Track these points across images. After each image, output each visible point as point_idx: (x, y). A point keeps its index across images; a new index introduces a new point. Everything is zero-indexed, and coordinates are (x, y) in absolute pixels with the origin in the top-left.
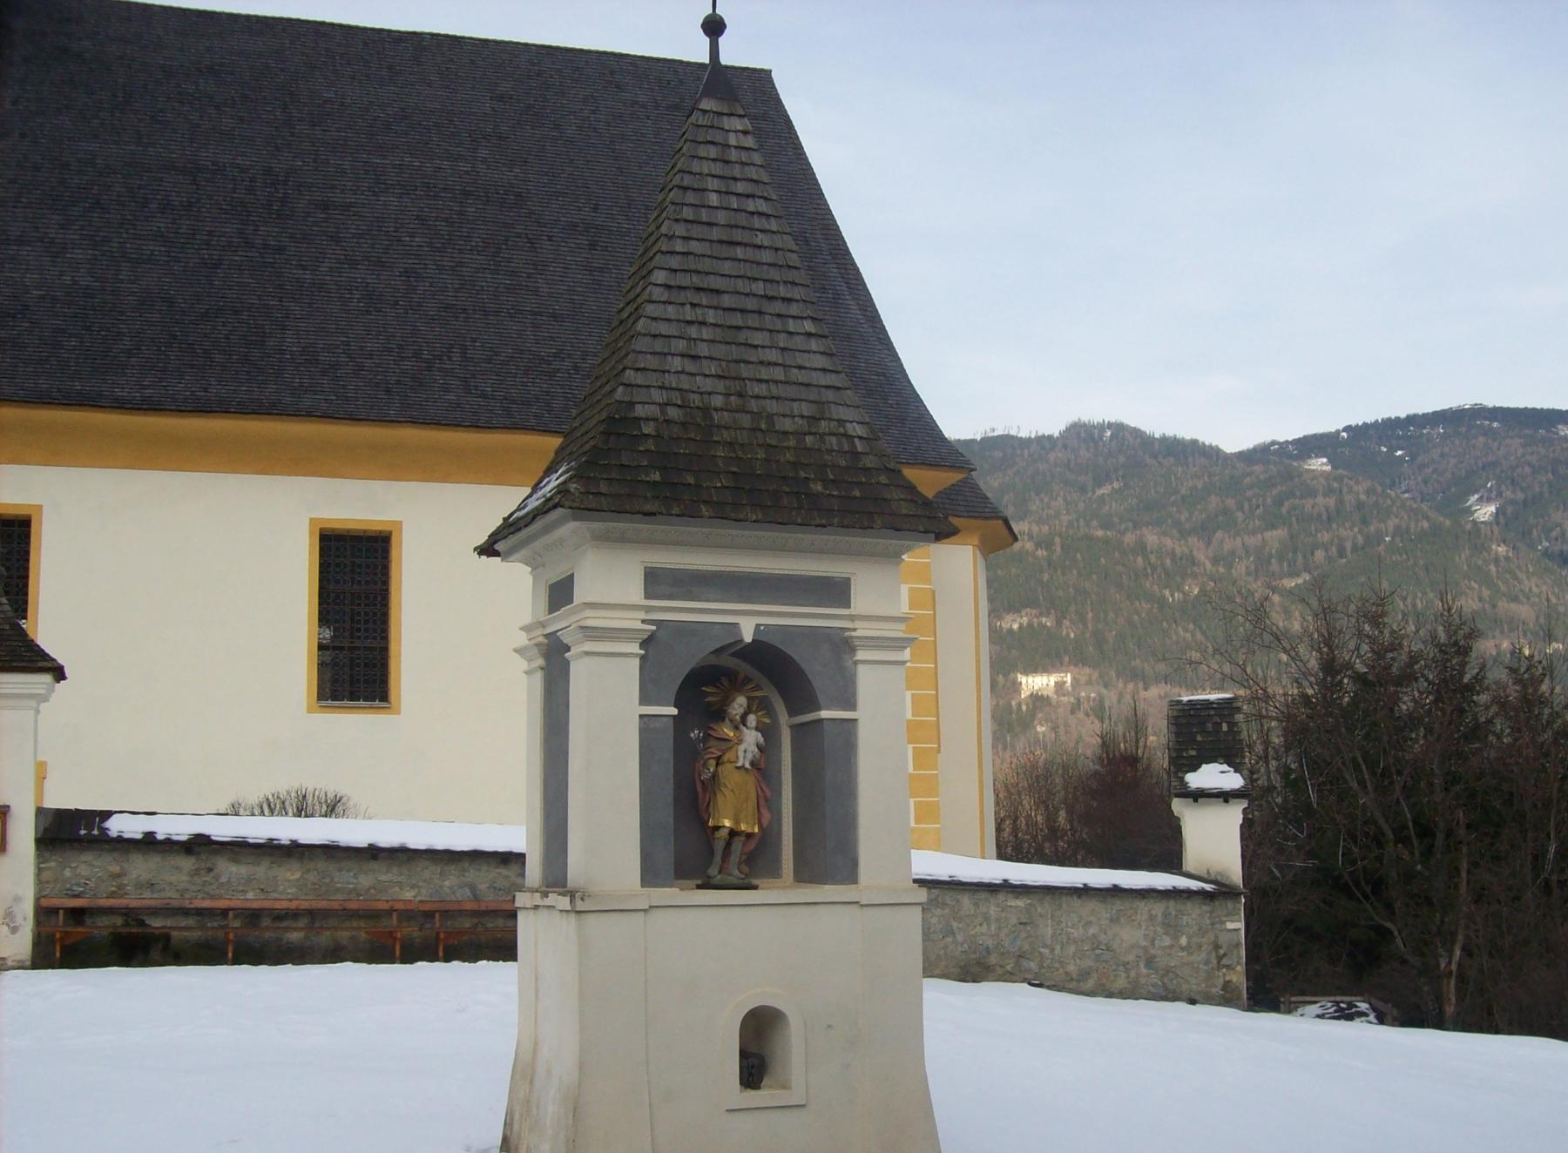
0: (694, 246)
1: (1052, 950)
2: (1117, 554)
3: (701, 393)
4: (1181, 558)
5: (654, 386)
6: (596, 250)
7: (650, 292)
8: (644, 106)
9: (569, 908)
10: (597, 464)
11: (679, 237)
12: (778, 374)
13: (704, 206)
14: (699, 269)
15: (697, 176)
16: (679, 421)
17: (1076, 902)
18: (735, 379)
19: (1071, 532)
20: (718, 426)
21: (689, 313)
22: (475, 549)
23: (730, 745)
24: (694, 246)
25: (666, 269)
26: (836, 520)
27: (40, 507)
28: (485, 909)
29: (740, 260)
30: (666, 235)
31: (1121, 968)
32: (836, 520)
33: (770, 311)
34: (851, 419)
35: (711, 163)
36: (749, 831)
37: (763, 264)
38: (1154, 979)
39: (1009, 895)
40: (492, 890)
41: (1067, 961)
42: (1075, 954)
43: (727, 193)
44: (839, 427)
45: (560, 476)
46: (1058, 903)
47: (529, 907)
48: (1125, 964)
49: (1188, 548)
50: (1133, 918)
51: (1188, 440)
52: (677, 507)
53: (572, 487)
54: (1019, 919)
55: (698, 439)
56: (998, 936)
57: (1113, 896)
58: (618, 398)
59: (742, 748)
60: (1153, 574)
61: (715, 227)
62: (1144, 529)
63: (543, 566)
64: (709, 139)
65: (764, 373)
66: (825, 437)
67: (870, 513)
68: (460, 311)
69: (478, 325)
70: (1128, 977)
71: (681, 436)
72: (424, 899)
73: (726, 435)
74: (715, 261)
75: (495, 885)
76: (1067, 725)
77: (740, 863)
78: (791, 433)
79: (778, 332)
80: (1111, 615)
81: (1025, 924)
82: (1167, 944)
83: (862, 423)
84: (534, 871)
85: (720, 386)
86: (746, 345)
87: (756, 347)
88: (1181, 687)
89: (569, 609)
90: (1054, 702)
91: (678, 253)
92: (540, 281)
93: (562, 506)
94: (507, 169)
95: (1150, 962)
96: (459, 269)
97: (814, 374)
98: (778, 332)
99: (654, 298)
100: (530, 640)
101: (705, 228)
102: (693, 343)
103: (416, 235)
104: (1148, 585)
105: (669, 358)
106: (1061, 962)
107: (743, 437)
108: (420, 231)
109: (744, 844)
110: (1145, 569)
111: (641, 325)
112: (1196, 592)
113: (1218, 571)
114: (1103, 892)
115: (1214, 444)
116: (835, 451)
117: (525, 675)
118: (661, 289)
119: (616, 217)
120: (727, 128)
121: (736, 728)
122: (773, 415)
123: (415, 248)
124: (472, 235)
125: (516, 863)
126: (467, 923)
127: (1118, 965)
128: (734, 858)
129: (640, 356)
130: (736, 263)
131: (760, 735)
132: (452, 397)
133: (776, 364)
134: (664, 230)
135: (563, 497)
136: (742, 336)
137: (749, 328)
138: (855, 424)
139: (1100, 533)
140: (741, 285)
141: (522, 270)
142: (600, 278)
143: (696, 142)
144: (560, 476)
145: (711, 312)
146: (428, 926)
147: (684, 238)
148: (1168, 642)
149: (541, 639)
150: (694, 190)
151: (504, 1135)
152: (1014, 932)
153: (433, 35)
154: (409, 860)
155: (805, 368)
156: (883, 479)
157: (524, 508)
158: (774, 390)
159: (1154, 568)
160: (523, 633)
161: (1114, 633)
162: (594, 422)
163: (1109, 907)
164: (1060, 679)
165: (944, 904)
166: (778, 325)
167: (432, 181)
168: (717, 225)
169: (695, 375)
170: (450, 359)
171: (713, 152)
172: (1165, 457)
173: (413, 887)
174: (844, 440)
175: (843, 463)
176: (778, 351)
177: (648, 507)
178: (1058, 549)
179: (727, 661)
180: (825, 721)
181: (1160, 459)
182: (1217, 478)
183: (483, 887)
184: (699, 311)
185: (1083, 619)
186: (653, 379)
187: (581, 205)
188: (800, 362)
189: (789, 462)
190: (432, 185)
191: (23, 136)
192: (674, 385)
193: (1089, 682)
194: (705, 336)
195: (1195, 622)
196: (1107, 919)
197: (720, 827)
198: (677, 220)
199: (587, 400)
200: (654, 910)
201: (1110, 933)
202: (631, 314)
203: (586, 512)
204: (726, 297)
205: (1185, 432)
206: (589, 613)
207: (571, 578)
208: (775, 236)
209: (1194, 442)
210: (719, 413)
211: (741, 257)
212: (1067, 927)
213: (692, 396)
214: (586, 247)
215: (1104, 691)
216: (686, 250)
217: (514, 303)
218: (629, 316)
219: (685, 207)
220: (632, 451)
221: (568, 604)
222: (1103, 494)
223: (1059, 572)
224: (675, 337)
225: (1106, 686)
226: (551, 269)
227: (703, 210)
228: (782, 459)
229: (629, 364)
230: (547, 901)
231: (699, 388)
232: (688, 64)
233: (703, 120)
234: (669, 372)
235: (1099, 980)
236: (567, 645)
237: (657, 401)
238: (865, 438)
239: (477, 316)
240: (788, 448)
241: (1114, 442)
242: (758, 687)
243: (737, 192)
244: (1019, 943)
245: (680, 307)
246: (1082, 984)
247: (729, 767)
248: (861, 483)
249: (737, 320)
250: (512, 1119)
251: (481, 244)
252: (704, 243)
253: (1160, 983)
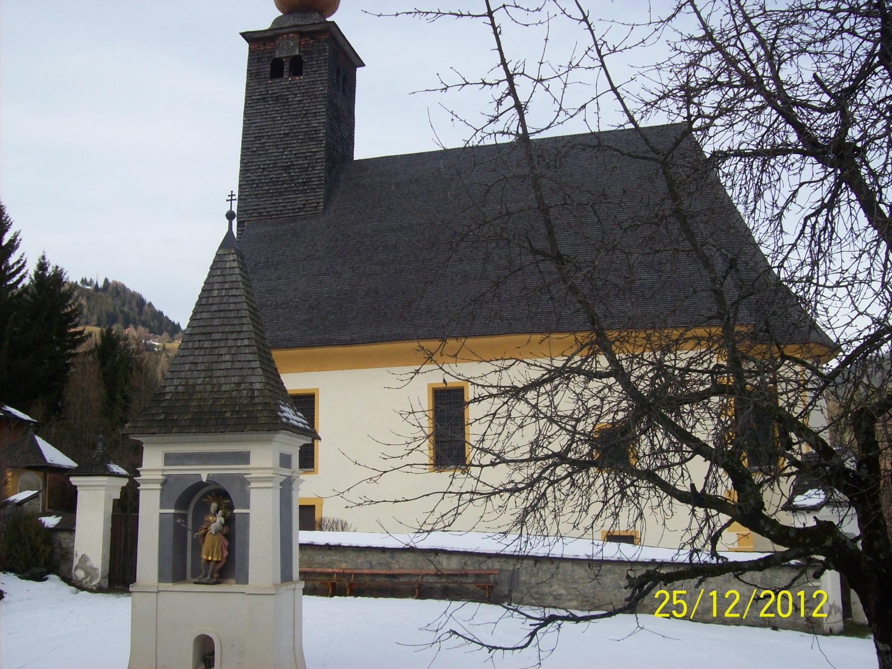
27: (318, 389)
165: (615, 573)
173: (346, 562)
177: (154, 431)
191: (335, 226)
200: (161, 593)
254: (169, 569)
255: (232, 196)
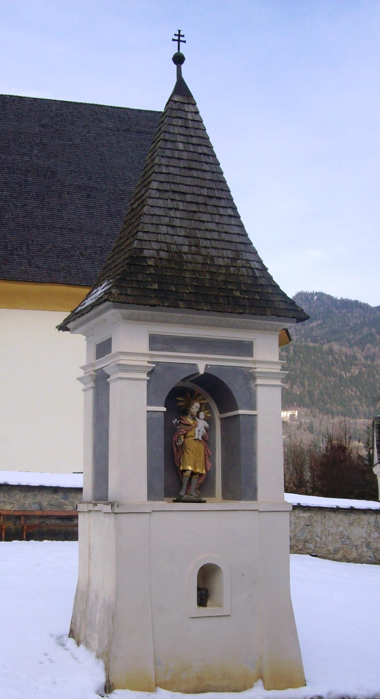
0: (172, 170)
1: (321, 539)
2: (319, 354)
3: (177, 245)
4: (350, 357)
5: (153, 241)
6: (90, 198)
7: (150, 192)
8: (111, 130)
9: (111, 511)
10: (125, 279)
11: (164, 165)
12: (216, 236)
13: (176, 150)
14: (175, 181)
15: (172, 134)
16: (165, 259)
17: (332, 515)
18: (193, 238)
19: (298, 344)
20: (186, 262)
21: (170, 204)
22: (57, 327)
23: (191, 427)
24: (172, 170)
25: (158, 181)
26: (248, 310)
28: (46, 515)
29: (195, 178)
30: (157, 164)
31: (354, 548)
32: (248, 310)
33: (210, 204)
34: (253, 260)
35: (179, 128)
36: (201, 472)
37: (206, 180)
38: (370, 553)
39: (301, 511)
40: (49, 505)
41: (328, 544)
42: (332, 540)
43: (188, 143)
44: (247, 263)
45: (104, 287)
46: (324, 515)
47: (86, 511)
48: (356, 546)
49: (353, 352)
50: (360, 523)
51: (353, 301)
52: (167, 302)
53: (113, 291)
54: (305, 523)
55: (176, 268)
56: (295, 531)
57: (351, 512)
58: (135, 247)
59: (197, 429)
60: (336, 364)
61: (182, 161)
62: (332, 342)
63: (93, 335)
64: (178, 115)
65: (208, 235)
66: (240, 268)
67: (265, 307)
68: (25, 227)
69: (35, 234)
70: (358, 552)
71: (167, 266)
72: (16, 509)
73: (190, 267)
74: (182, 177)
75: (51, 503)
76: (295, 434)
77: (196, 489)
78: (223, 266)
79: (215, 214)
80: (317, 384)
81: (308, 525)
82: (377, 536)
83: (258, 262)
84: (88, 494)
85: (186, 241)
86: (199, 220)
87: (204, 222)
88: (349, 418)
89: (101, 360)
90: (289, 424)
91: (164, 173)
92: (64, 213)
93: (109, 301)
94: (47, 160)
95: (368, 545)
96: (25, 207)
97: (233, 236)
98: (215, 214)
99: (152, 196)
100: (85, 373)
101: (177, 161)
102: (172, 219)
103: (4, 191)
104: (334, 370)
105: (160, 226)
106: (325, 545)
107: (199, 267)
108: (6, 189)
109: (199, 479)
110: (333, 361)
111: (146, 209)
112: (357, 373)
113: (367, 362)
114: (346, 511)
115: (366, 303)
116: (245, 276)
117: (83, 392)
118: (155, 192)
119: (100, 182)
120: (187, 110)
121: (194, 419)
122: (214, 256)
123: (4, 197)
124: (31, 191)
125: (61, 492)
126: (37, 522)
127: (352, 546)
128: (193, 486)
129: (146, 225)
130: (193, 179)
131: (206, 422)
132: (23, 268)
133: (214, 231)
134: (156, 161)
135: (109, 296)
136: (197, 216)
137: (200, 212)
138: (255, 262)
139: (312, 344)
140: (196, 190)
141: (55, 208)
142: (92, 212)
143: (171, 117)
144: (104, 287)
145: (181, 203)
146: (18, 523)
147: (166, 166)
148: (344, 396)
149: (92, 373)
150: (171, 141)
151: (70, 628)
152: (303, 529)
153: (11, 96)
154: (9, 490)
155: (229, 233)
156: (270, 291)
157: (83, 305)
158: (214, 244)
159: (337, 361)
160: (82, 371)
161: (318, 392)
162: (122, 260)
163: (349, 517)
164: (292, 413)
166: (215, 211)
167: (11, 165)
168: (183, 159)
169: (173, 235)
170: (21, 249)
171: (180, 122)
172: (342, 309)
173: (10, 503)
174: (250, 270)
175: (250, 282)
176: (215, 224)
177: (152, 302)
178: (292, 352)
179: (189, 385)
180: (241, 415)
181: (340, 309)
182: (367, 319)
183: (45, 504)
184: (175, 203)
185: (303, 386)
186: (152, 237)
187: (83, 177)
188: (226, 230)
189: (222, 281)
190: (11, 167)
192: (163, 240)
193: (306, 415)
194: (178, 216)
195: (356, 387)
196: (348, 523)
197: (187, 470)
198: (163, 157)
199: (115, 250)
201: (349, 530)
202: (139, 205)
203: (120, 304)
204: (188, 196)
205: (352, 297)
206: (121, 357)
207: (110, 340)
208: (212, 166)
209: (356, 302)
210: (186, 255)
211: (195, 176)
212: (328, 527)
213: (173, 246)
214: (86, 197)
215: (313, 419)
216: (167, 172)
217: (51, 223)
218: (137, 206)
219: (166, 150)
220: (143, 273)
221: (109, 353)
222: (313, 326)
223: (292, 363)
224: (163, 216)
225: (314, 417)
226: (69, 207)
227: (176, 151)
228: (219, 279)
229: (140, 229)
230: (97, 508)
231: (176, 242)
232: (133, 110)
233: (175, 106)
234: (160, 233)
235: (343, 554)
236: (108, 374)
237: (155, 248)
238: (260, 269)
239: (34, 229)
240: (222, 274)
241: (318, 302)
242: (204, 399)
243: (193, 143)
244: (305, 535)
245: (165, 201)
246: (335, 555)
247: (191, 439)
248: (259, 292)
249: (194, 208)
250: (76, 620)
251: (35, 195)
252: (176, 168)
253: (373, 556)
254: (160, 485)
255: (179, 36)
